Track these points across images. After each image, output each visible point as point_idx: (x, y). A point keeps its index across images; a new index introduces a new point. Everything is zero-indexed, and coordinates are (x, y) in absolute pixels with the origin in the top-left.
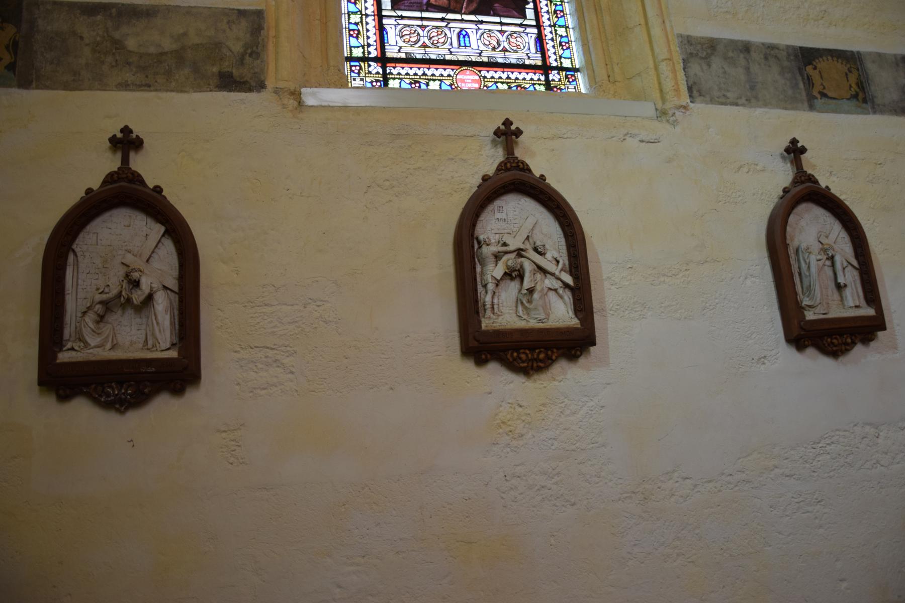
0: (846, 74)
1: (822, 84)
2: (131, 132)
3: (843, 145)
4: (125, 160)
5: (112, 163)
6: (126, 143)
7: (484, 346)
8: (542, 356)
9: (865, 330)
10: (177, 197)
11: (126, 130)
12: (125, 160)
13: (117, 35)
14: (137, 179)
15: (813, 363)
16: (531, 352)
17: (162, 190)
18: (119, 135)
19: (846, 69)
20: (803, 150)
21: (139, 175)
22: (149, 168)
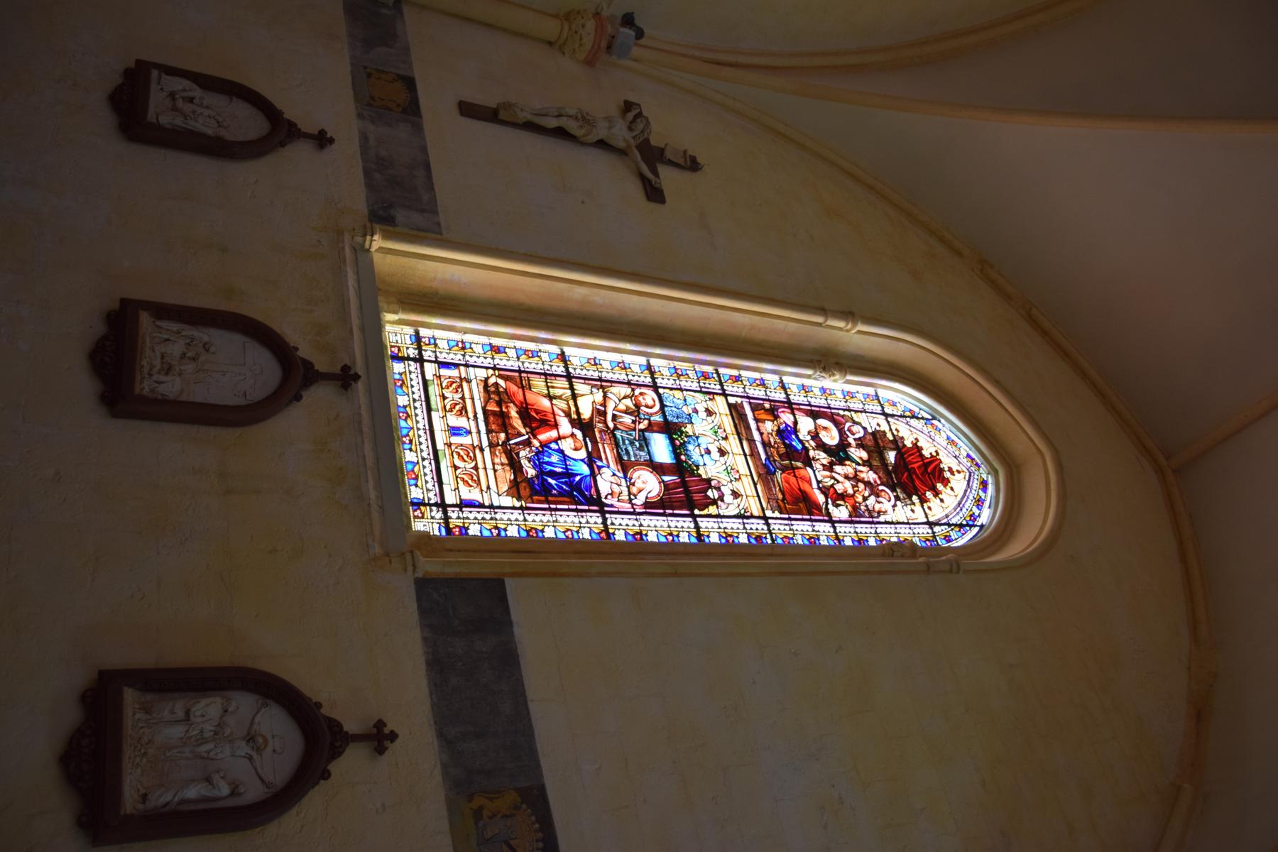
2: (392, 741)
6: (322, 140)
7: (102, 698)
10: (314, 800)
11: (393, 736)
14: (336, 753)
15: (81, 325)
16: (90, 757)
18: (386, 730)
20: (381, 750)
21: (340, 754)
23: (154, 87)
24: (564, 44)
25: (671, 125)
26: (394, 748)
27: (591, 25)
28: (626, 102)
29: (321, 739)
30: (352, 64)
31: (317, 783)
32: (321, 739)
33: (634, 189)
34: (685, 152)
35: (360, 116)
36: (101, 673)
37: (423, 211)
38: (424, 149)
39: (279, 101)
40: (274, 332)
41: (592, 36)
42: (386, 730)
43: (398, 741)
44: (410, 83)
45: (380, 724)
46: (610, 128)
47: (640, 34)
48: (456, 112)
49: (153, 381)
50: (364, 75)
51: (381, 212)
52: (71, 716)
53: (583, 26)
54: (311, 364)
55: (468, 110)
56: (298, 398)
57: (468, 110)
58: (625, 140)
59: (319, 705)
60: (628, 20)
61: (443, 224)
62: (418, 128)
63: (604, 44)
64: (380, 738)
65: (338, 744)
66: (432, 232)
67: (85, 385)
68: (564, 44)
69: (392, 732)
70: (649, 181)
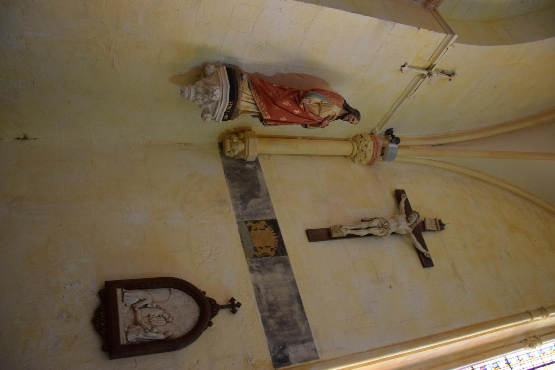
0: (269, 247)
1: (257, 229)
2: (239, 307)
3: (240, 337)
4: (223, 307)
5: (220, 301)
6: (233, 306)
7: (108, 293)
8: (103, 324)
9: (112, 345)
10: (207, 334)
11: (239, 305)
12: (223, 307)
13: (255, 149)
14: (214, 314)
15: (86, 303)
16: (105, 320)
17: (210, 326)
18: (236, 302)
19: (272, 246)
20: (234, 312)
21: (216, 314)
22: (221, 319)
23: (120, 306)
24: (355, 157)
25: (426, 200)
26: (240, 310)
27: (371, 144)
28: (396, 191)
29: (207, 309)
30: (238, 223)
31: (206, 328)
32: (207, 309)
33: (415, 261)
34: (435, 219)
35: (251, 270)
36: (106, 282)
37: (303, 342)
38: (294, 284)
39: (201, 286)
40: (201, 334)
41: (372, 151)
42: (236, 302)
43: (241, 307)
44: (274, 224)
45: (233, 300)
46: (398, 226)
47: (397, 140)
48: (305, 238)
49: (128, 335)
50: (248, 227)
51: (279, 356)
52: (94, 301)
53: (366, 146)
54: (214, 301)
55: (314, 235)
56: (210, 324)
57: (314, 235)
58: (406, 230)
59: (204, 293)
60: (389, 132)
61: (318, 349)
62: (287, 265)
63: (379, 154)
64: (233, 306)
65: (215, 310)
66: (313, 359)
67: (91, 340)
68: (355, 157)
69: (238, 303)
70: (423, 254)
